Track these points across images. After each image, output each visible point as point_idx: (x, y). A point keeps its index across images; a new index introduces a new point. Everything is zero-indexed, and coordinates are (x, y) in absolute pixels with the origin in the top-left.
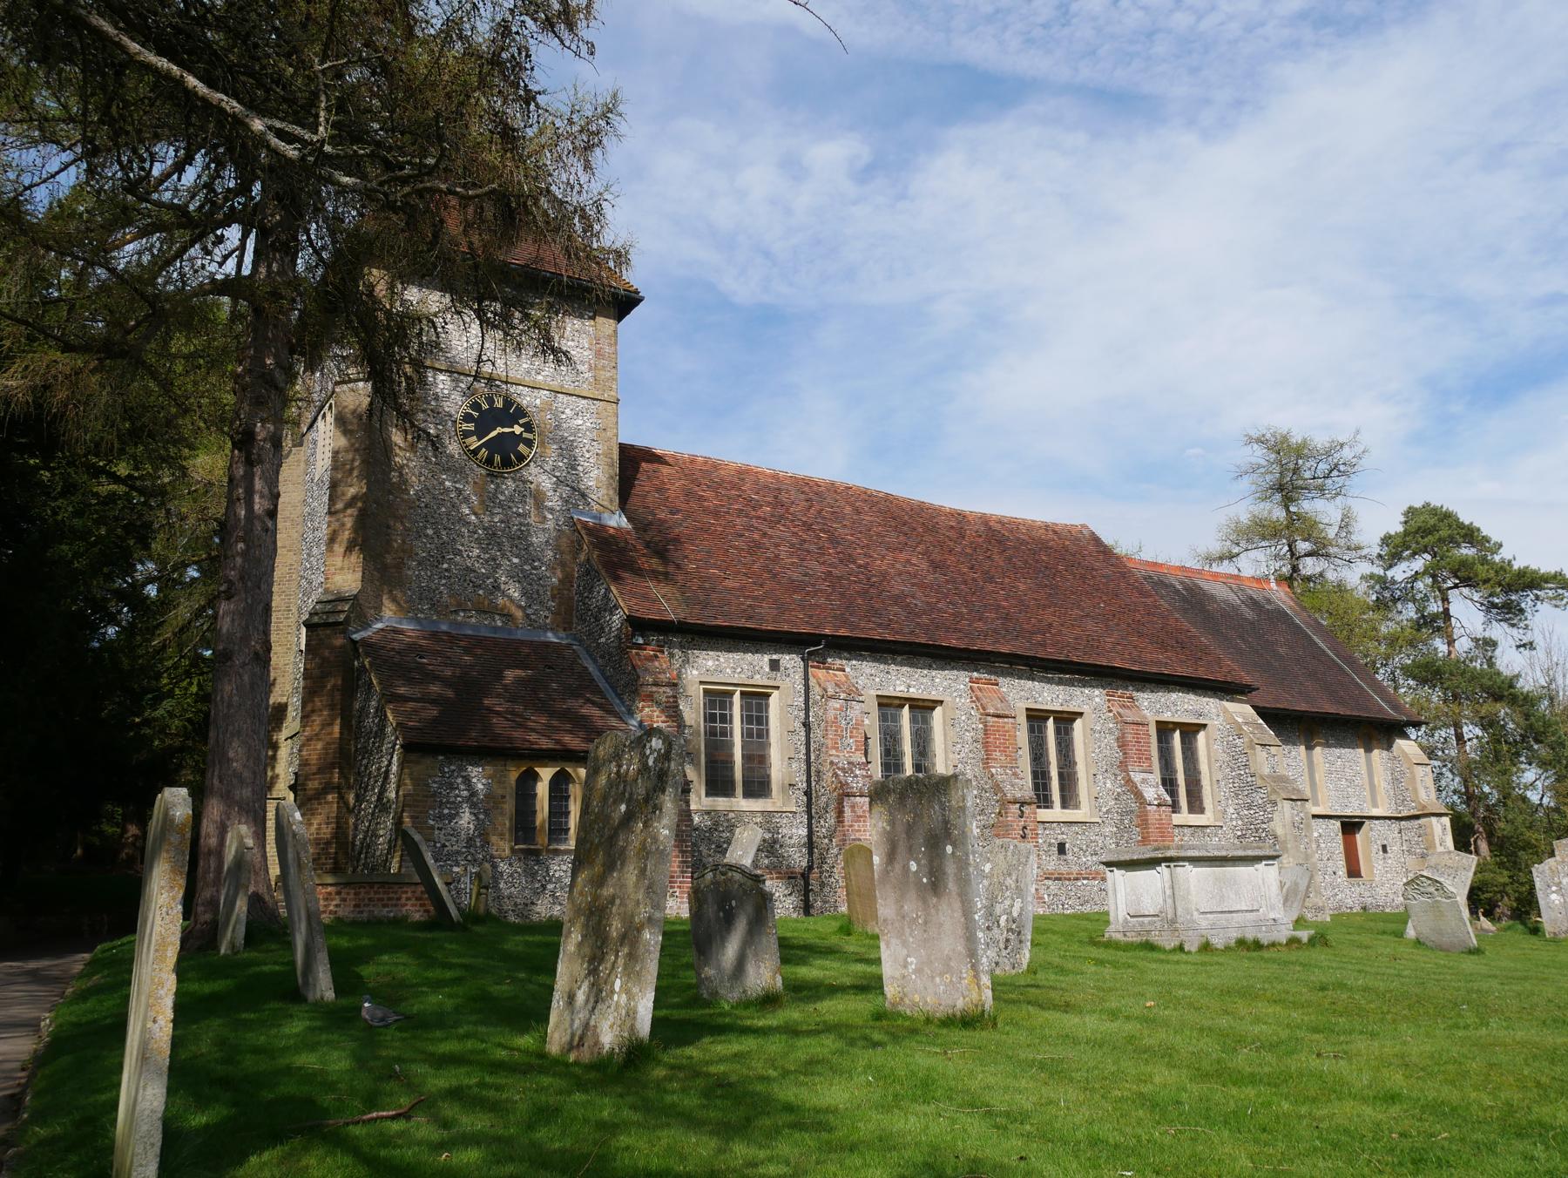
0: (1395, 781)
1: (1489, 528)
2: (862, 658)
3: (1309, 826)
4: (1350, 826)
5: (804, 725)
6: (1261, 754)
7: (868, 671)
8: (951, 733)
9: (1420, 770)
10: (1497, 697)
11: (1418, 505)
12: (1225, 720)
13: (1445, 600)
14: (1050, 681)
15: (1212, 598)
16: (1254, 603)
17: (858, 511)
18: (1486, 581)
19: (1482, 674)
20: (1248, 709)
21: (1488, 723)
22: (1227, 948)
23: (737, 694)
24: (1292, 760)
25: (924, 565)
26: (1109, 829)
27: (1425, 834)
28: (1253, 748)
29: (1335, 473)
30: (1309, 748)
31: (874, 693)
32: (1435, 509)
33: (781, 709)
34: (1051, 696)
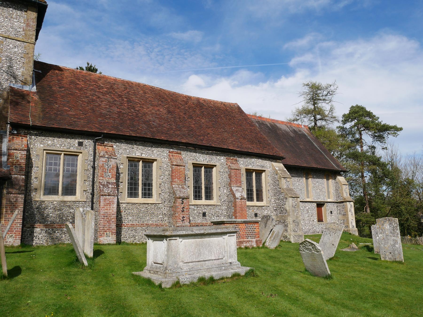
0: (337, 190)
1: (375, 113)
2: (121, 142)
3: (298, 206)
4: (320, 205)
5: (92, 167)
6: (283, 181)
7: (124, 147)
8: (160, 171)
9: (344, 187)
10: (374, 164)
11: (354, 105)
12: (272, 169)
13: (361, 134)
14: (203, 153)
15: (280, 129)
16: (295, 132)
17: (145, 93)
18: (373, 128)
19: (370, 157)
20: (281, 165)
21: (373, 172)
22: (193, 284)
23: (63, 154)
24: (298, 184)
25: (165, 112)
26: (224, 208)
27: (345, 208)
28: (281, 179)
29: (329, 94)
30: (307, 179)
31: (126, 156)
32: (359, 106)
33: (82, 161)
34: (203, 159)
